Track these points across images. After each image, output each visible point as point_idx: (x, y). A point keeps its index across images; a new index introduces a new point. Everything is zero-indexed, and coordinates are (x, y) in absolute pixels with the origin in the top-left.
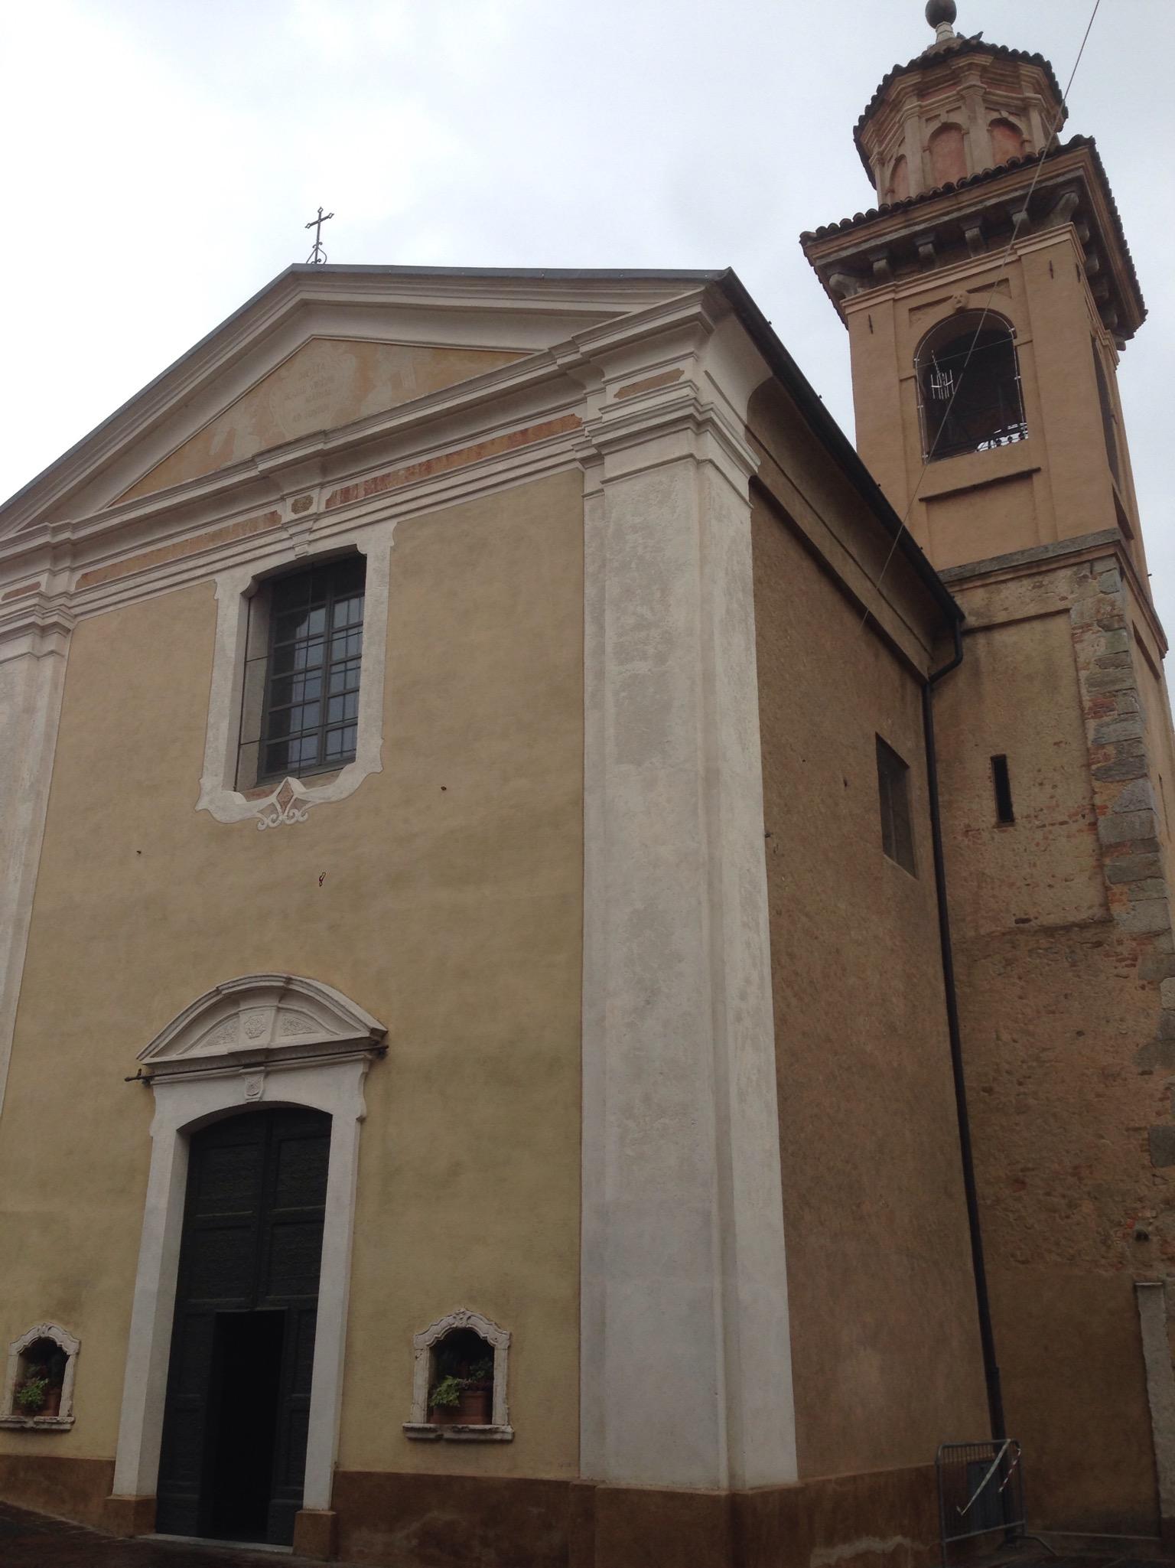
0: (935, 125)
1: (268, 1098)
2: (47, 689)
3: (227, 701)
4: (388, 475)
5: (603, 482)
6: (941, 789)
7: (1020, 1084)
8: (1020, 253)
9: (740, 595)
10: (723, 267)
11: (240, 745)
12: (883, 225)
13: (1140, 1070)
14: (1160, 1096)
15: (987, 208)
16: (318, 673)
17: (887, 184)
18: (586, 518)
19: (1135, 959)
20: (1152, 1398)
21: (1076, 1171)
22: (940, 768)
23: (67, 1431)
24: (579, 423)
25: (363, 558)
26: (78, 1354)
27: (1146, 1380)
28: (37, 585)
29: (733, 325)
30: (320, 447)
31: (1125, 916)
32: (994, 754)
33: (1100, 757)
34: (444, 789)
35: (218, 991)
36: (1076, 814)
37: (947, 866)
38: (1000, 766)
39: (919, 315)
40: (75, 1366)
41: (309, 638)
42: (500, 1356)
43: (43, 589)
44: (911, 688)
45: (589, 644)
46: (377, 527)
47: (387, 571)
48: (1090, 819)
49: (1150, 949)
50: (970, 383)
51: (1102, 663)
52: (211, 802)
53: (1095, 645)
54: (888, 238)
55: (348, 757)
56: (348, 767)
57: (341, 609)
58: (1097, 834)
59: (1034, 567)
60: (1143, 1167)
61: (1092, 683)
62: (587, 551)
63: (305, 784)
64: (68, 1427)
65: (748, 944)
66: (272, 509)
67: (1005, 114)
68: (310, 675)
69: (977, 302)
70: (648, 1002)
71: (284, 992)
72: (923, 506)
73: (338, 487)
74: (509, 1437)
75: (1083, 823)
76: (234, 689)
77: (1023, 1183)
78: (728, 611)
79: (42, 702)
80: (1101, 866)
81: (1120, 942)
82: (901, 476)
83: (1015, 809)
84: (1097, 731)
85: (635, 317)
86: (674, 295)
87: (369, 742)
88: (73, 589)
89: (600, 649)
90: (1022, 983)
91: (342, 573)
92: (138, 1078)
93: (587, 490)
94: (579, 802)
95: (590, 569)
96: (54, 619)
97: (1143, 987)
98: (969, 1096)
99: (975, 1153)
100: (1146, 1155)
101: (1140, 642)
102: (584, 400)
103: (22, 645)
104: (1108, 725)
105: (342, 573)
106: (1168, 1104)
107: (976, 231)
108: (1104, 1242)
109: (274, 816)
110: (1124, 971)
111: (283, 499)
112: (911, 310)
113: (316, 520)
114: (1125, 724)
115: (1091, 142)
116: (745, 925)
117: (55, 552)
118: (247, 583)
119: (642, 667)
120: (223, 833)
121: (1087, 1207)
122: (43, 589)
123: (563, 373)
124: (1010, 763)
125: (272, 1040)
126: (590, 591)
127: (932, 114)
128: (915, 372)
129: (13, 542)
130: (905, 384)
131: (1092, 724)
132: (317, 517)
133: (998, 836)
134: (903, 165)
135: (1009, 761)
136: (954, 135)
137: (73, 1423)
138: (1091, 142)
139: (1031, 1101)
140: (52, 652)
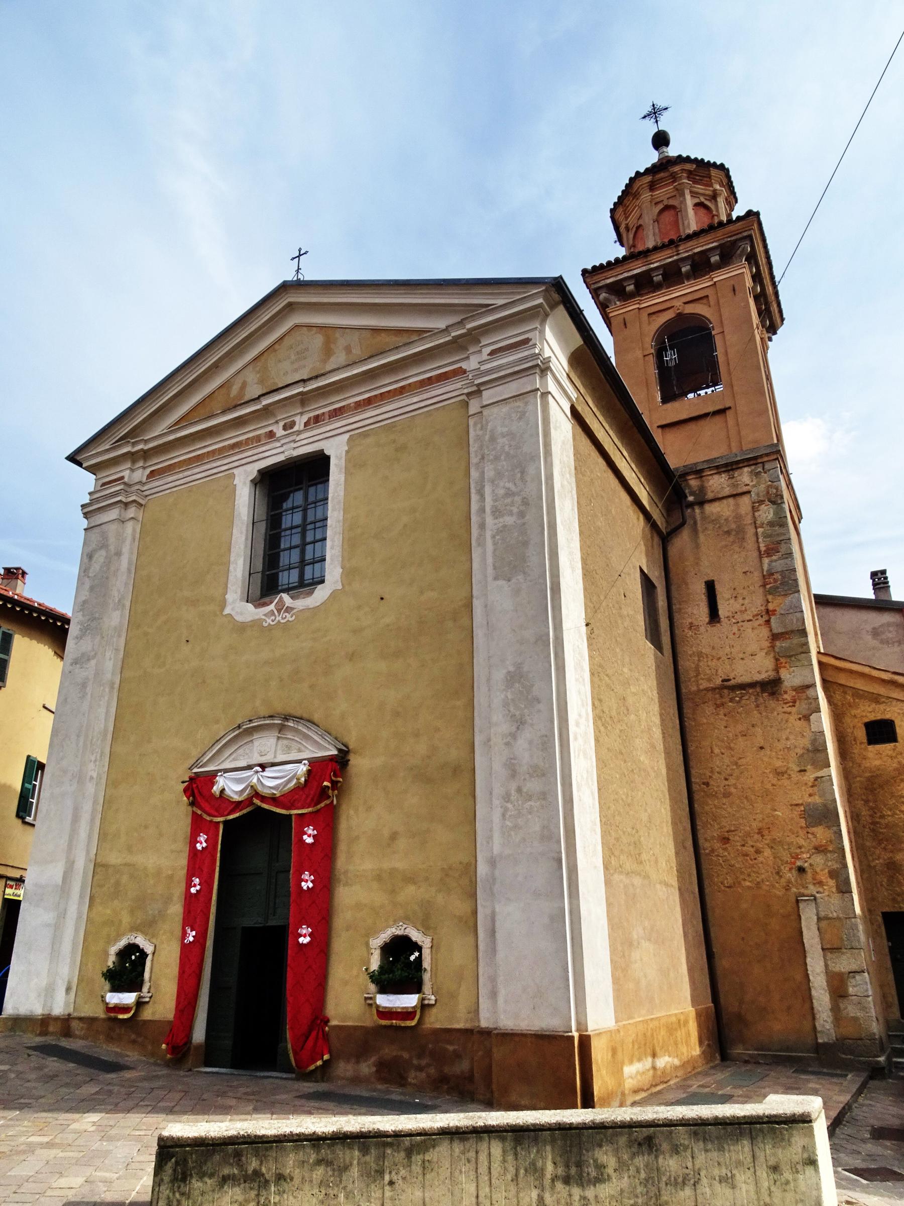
0: (661, 206)
2: (128, 542)
3: (242, 547)
5: (482, 407)
6: (674, 601)
7: (726, 779)
8: (715, 280)
9: (568, 476)
10: (557, 276)
11: (250, 574)
13: (799, 769)
14: (811, 784)
15: (695, 254)
16: (299, 530)
17: (631, 242)
19: (795, 702)
20: (809, 968)
21: (760, 832)
22: (673, 588)
24: (465, 372)
25: (328, 458)
26: (154, 954)
27: (805, 957)
28: (123, 478)
29: (561, 312)
30: (301, 390)
31: (788, 676)
32: (706, 579)
34: (382, 599)
35: (239, 727)
36: (757, 615)
37: (680, 649)
38: (710, 588)
39: (654, 317)
40: (152, 960)
41: (293, 508)
43: (126, 480)
44: (656, 539)
45: (474, 507)
46: (337, 438)
47: (344, 465)
48: (766, 618)
49: (804, 696)
51: (771, 524)
52: (232, 609)
54: (636, 272)
56: (320, 587)
57: (312, 490)
58: (770, 627)
59: (730, 467)
60: (801, 828)
61: (766, 536)
62: (472, 449)
63: (292, 598)
64: (147, 1000)
65: (579, 692)
66: (270, 429)
67: (702, 199)
68: (294, 531)
69: (689, 309)
70: (518, 728)
72: (660, 430)
73: (312, 414)
74: (433, 1002)
75: (761, 621)
76: (246, 539)
77: (728, 839)
79: (126, 550)
80: (773, 647)
81: (786, 692)
83: (720, 613)
84: (769, 565)
85: (501, 306)
86: (525, 292)
87: (333, 572)
88: (144, 480)
89: (482, 510)
90: (726, 718)
91: (315, 467)
93: (471, 413)
94: (469, 606)
95: (474, 460)
96: (134, 498)
97: (800, 719)
98: (695, 787)
99: (698, 823)
100: (803, 820)
102: (468, 358)
103: (113, 514)
104: (776, 561)
105: (315, 467)
106: (815, 788)
107: (688, 267)
108: (778, 873)
109: (273, 618)
110: (789, 709)
111: (277, 422)
112: (649, 314)
113: (298, 435)
114: (786, 561)
115: (757, 214)
116: (577, 680)
117: (132, 457)
118: (254, 474)
119: (509, 520)
120: (242, 628)
121: (767, 852)
122: (126, 480)
123: (455, 340)
124: (718, 587)
125: (275, 757)
126: (474, 474)
127: (658, 200)
128: (653, 351)
129: (107, 451)
130: (647, 358)
131: (766, 561)
132: (299, 432)
133: (709, 628)
134: (640, 231)
135: (716, 583)
136: (672, 212)
137: (151, 997)
138: (757, 214)
139: (733, 790)
140: (132, 518)
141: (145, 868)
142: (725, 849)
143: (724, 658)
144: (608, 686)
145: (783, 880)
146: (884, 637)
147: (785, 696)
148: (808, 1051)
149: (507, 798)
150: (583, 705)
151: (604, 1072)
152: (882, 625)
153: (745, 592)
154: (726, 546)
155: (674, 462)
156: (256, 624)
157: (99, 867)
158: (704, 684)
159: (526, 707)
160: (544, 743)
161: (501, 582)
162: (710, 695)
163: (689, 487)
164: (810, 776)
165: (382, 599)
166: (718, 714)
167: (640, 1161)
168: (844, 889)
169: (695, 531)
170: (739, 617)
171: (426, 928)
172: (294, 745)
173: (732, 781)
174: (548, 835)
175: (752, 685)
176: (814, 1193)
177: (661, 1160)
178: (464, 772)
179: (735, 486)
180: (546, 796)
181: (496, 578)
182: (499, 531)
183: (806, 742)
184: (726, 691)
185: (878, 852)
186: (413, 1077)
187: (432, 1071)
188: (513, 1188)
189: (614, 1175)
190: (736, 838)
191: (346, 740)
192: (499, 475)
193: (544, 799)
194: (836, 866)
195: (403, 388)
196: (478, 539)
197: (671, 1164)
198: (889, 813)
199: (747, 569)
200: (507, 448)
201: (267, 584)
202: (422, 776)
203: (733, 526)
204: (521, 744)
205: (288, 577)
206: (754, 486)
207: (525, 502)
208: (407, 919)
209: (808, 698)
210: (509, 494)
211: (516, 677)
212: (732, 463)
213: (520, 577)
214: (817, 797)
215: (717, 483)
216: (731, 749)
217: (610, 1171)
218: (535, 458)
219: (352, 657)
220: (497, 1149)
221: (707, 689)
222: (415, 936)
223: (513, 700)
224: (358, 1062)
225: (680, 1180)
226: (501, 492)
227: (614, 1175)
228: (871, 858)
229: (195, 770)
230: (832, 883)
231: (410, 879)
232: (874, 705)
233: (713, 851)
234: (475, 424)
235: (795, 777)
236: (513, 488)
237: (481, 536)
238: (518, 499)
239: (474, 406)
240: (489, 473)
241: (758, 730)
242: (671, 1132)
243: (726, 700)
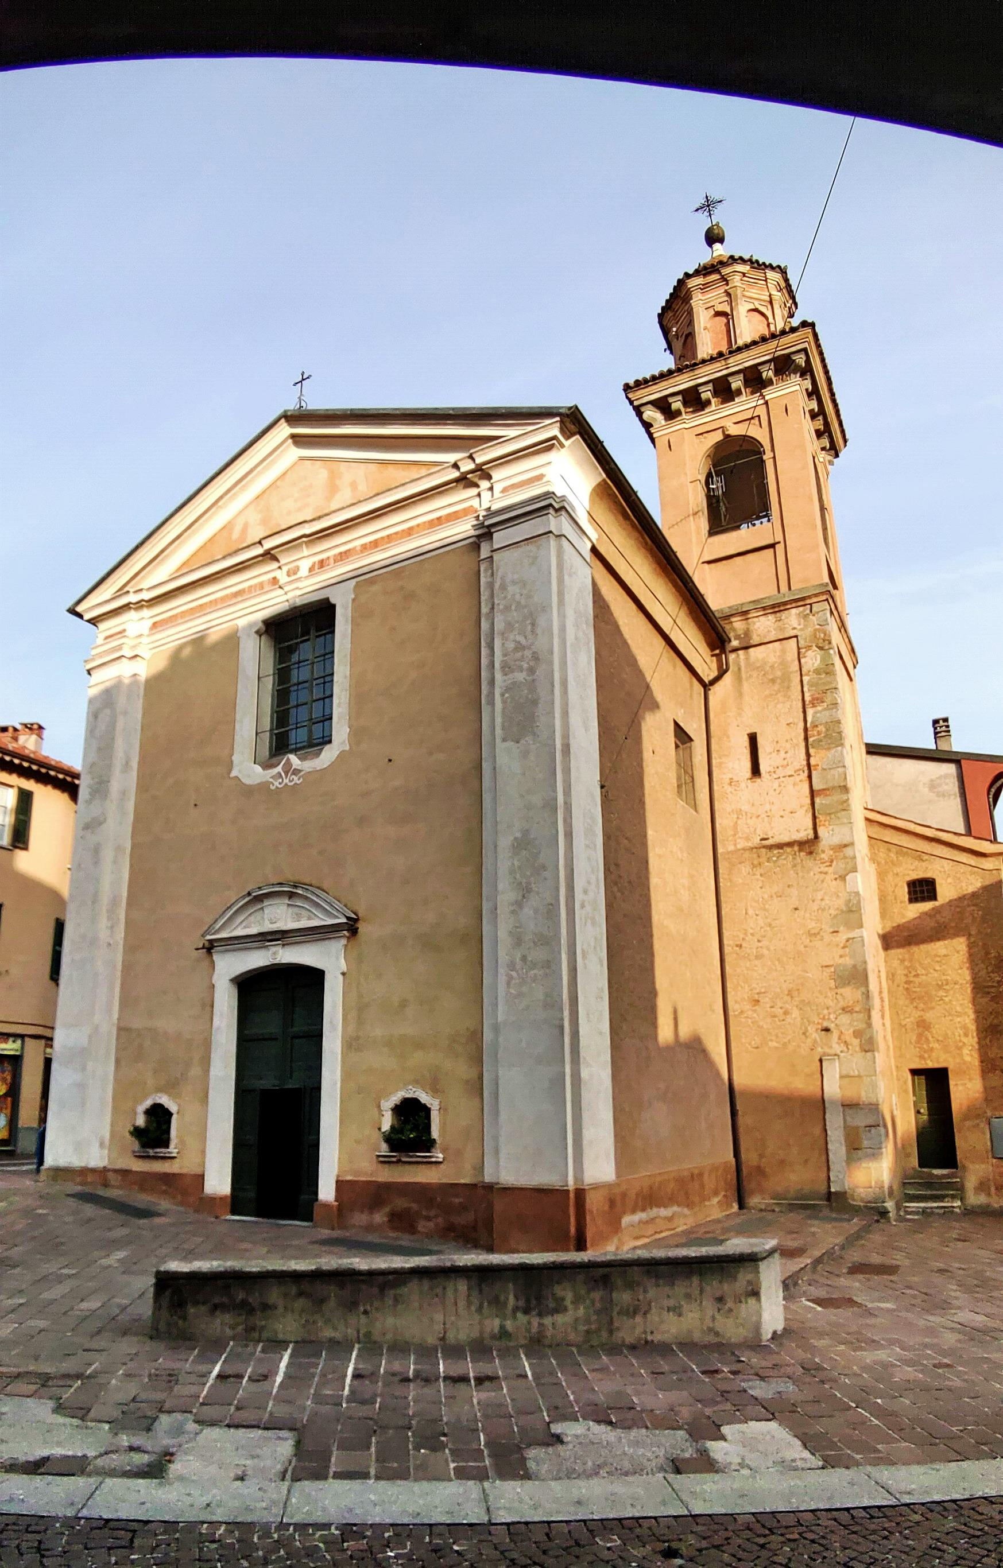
1: (283, 962)
4: (349, 550)
7: (759, 941)
12: (677, 379)
16: (306, 685)
18: (482, 575)
19: (832, 862)
23: (174, 1158)
25: (334, 606)
32: (749, 731)
33: (815, 733)
34: (390, 760)
35: (249, 894)
42: (435, 1116)
45: (484, 661)
50: (739, 484)
51: (817, 672)
53: (813, 660)
55: (327, 740)
56: (327, 747)
59: (777, 608)
60: (830, 989)
62: (483, 598)
63: (299, 759)
65: (589, 859)
68: (300, 687)
70: (524, 896)
71: (291, 892)
78: (576, 639)
81: (823, 852)
82: (691, 540)
87: (341, 731)
89: (492, 665)
92: (203, 948)
93: (482, 557)
97: (836, 879)
98: (727, 950)
101: (841, 657)
104: (820, 712)
106: (847, 950)
108: (804, 1034)
110: (823, 869)
116: (587, 846)
119: (520, 676)
120: (248, 791)
121: (796, 1013)
126: (485, 625)
134: (690, 338)
139: (765, 952)
141: (166, 1033)
142: (755, 1011)
143: (763, 816)
144: (626, 849)
145: (809, 1040)
146: (940, 789)
147: (823, 856)
148: (821, 1199)
149: (512, 966)
150: (593, 872)
151: (599, 1222)
152: (940, 778)
153: (788, 745)
154: (771, 695)
155: (716, 602)
156: (264, 786)
157: (122, 1030)
158: (742, 844)
159: (532, 875)
160: (549, 912)
161: (510, 744)
162: (747, 855)
163: (734, 630)
164: (843, 937)
165: (390, 760)
166: (754, 875)
167: (596, 1295)
168: (869, 1046)
169: (739, 678)
170: (780, 772)
171: (435, 1089)
172: (304, 913)
173: (765, 943)
174: (552, 1003)
175: (790, 844)
176: (754, 1318)
177: (614, 1295)
178: (473, 940)
179: (782, 629)
180: (550, 965)
181: (504, 740)
182: (508, 689)
183: (840, 903)
184: (763, 850)
185: (909, 1010)
186: (422, 1226)
187: (440, 1220)
188: (477, 1317)
189: (570, 1306)
190: (765, 1000)
191: (355, 908)
192: (510, 626)
193: (549, 967)
194: (862, 1026)
195: (411, 529)
196: (488, 696)
197: (624, 1297)
198: (924, 972)
199: (791, 720)
200: (517, 597)
201: (280, 744)
202: (428, 943)
203: (779, 673)
204: (527, 911)
205: (297, 736)
206: (801, 630)
207: (536, 657)
208: (416, 1082)
209: (845, 857)
210: (519, 647)
211: (523, 844)
212: (779, 605)
213: (529, 739)
214: (847, 958)
215: (763, 626)
216: (765, 910)
217: (568, 1302)
218: (545, 608)
219: (362, 821)
220: (462, 1286)
221: (744, 849)
222: (424, 1098)
223: (519, 867)
224: (371, 1213)
225: (631, 1309)
226: (511, 645)
227: (570, 1306)
228: (902, 1017)
229: (209, 937)
230: (856, 1042)
231: (419, 1045)
232: (917, 863)
233: (742, 1012)
234: (486, 571)
235: (828, 938)
236: (523, 641)
237: (491, 694)
238: (528, 653)
239: (485, 552)
240: (499, 625)
241: (794, 892)
242: (625, 1272)
243: (763, 859)
